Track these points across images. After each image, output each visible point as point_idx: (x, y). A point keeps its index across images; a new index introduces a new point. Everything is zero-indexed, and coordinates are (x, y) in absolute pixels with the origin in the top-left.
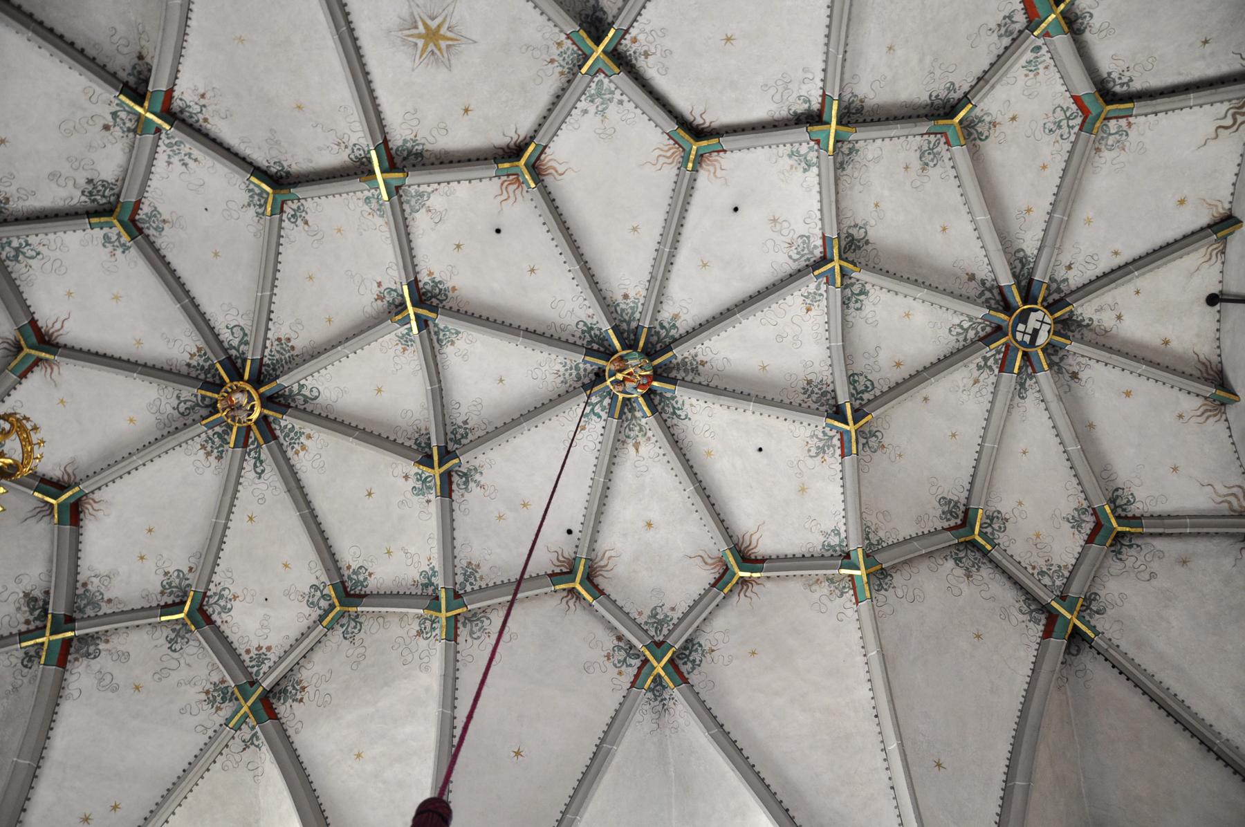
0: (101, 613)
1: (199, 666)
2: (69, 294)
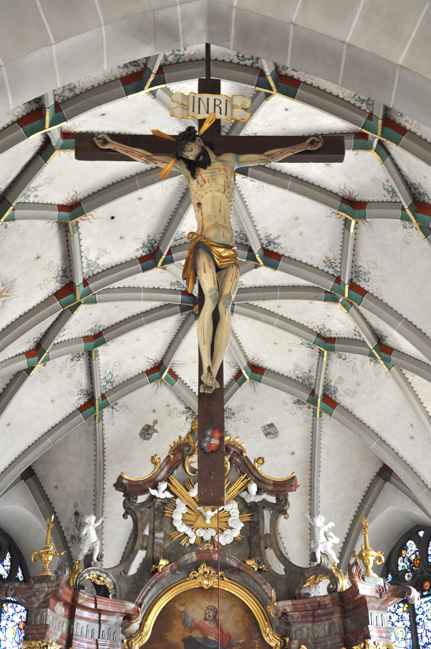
2: (133, 357)
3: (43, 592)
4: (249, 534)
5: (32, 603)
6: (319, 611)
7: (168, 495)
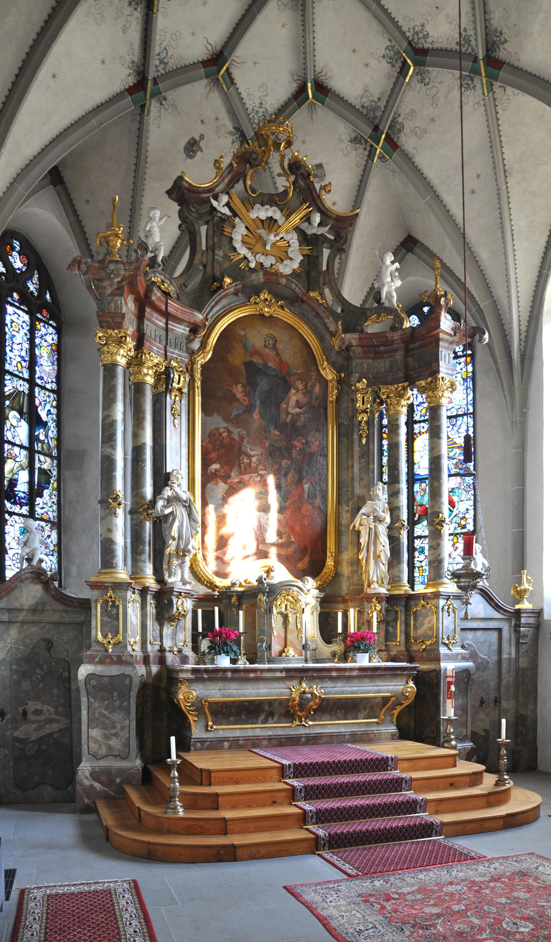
0: (383, 108)
1: (445, 79)
2: (193, 34)
3: (118, 275)
4: (307, 268)
5: (104, 288)
6: (382, 348)
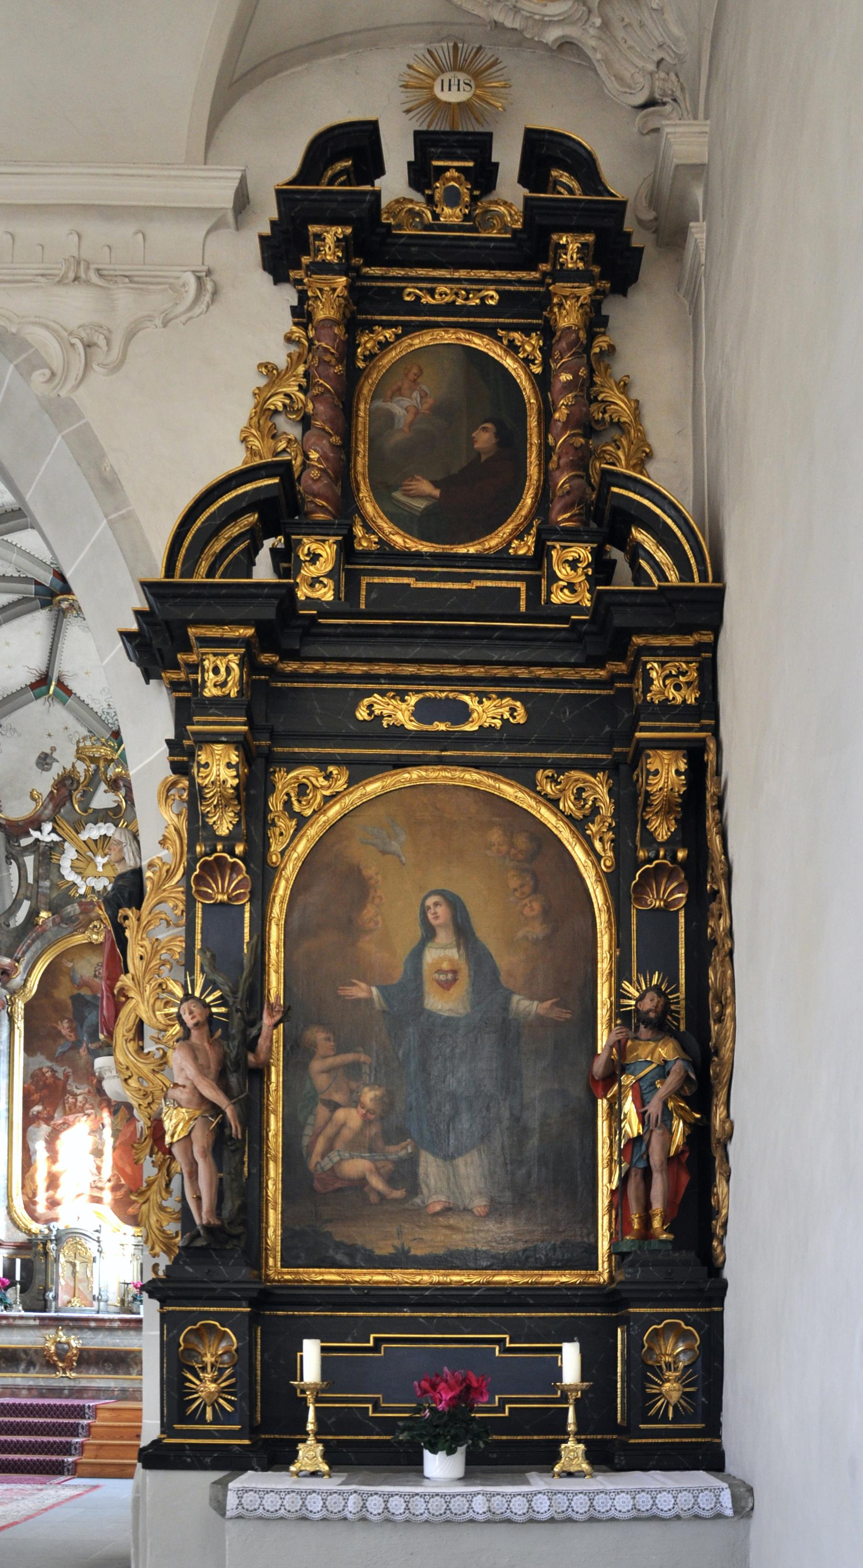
7: (55, 837)
